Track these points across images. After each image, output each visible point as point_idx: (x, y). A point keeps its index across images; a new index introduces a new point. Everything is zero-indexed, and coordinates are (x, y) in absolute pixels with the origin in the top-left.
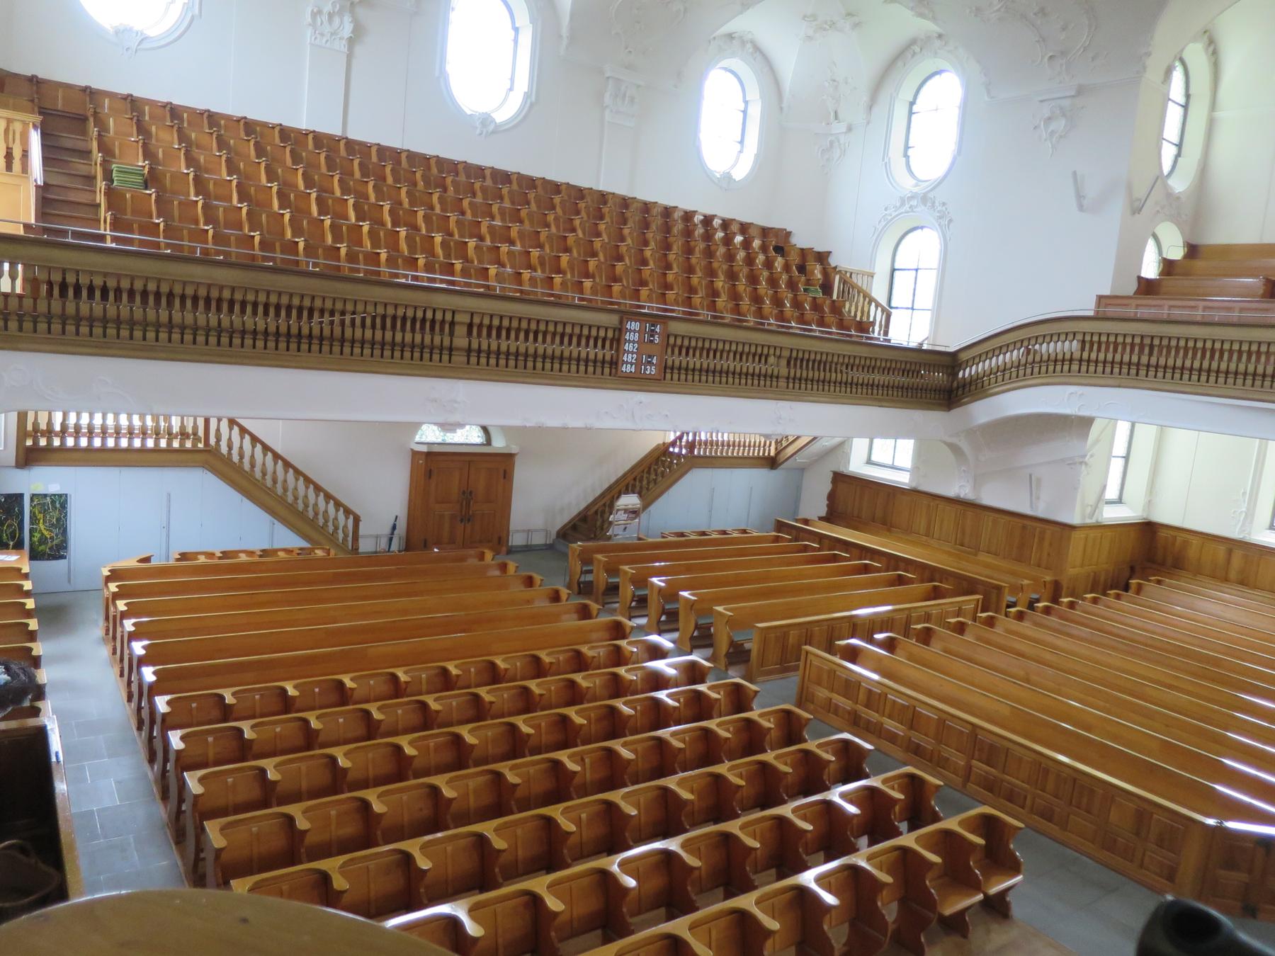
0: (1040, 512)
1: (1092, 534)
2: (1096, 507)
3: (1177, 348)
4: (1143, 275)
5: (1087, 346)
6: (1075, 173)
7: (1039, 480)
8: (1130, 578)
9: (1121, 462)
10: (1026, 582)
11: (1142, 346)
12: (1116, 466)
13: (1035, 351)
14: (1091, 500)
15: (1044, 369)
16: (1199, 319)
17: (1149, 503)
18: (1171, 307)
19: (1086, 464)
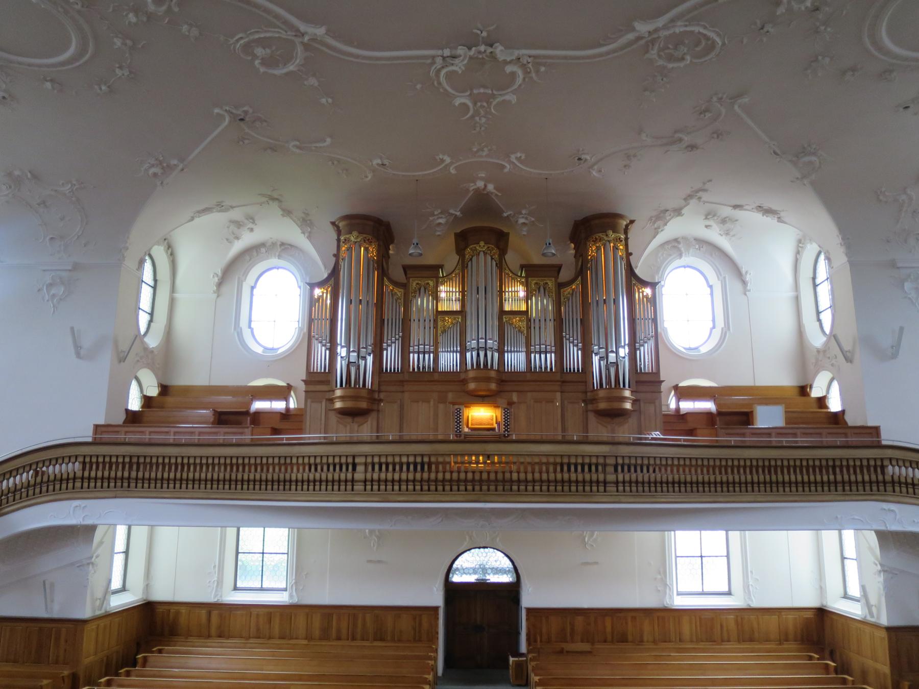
0: (56, 614)
1: (102, 623)
2: (104, 598)
3: (151, 464)
4: (130, 408)
5: (88, 466)
6: (72, 329)
7: (52, 585)
8: (137, 654)
9: (122, 556)
10: (45, 682)
11: (131, 463)
12: (118, 560)
13: (43, 473)
14: (99, 594)
15: (51, 488)
16: (171, 441)
17: (147, 587)
18: (150, 433)
19: (93, 564)
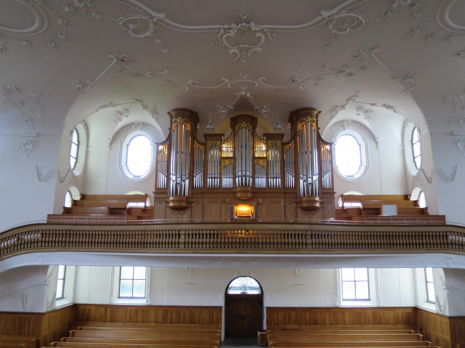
0: (28, 310)
1: (51, 315)
2: (53, 302)
3: (76, 234)
4: (66, 206)
5: (44, 235)
6: (37, 166)
7: (26, 295)
8: (69, 331)
9: (62, 281)
10: (23, 344)
11: (66, 234)
12: (60, 283)
13: (22, 239)
14: (50, 300)
15: (26, 246)
16: (87, 223)
17: (75, 297)
18: (76, 219)
19: (47, 285)
